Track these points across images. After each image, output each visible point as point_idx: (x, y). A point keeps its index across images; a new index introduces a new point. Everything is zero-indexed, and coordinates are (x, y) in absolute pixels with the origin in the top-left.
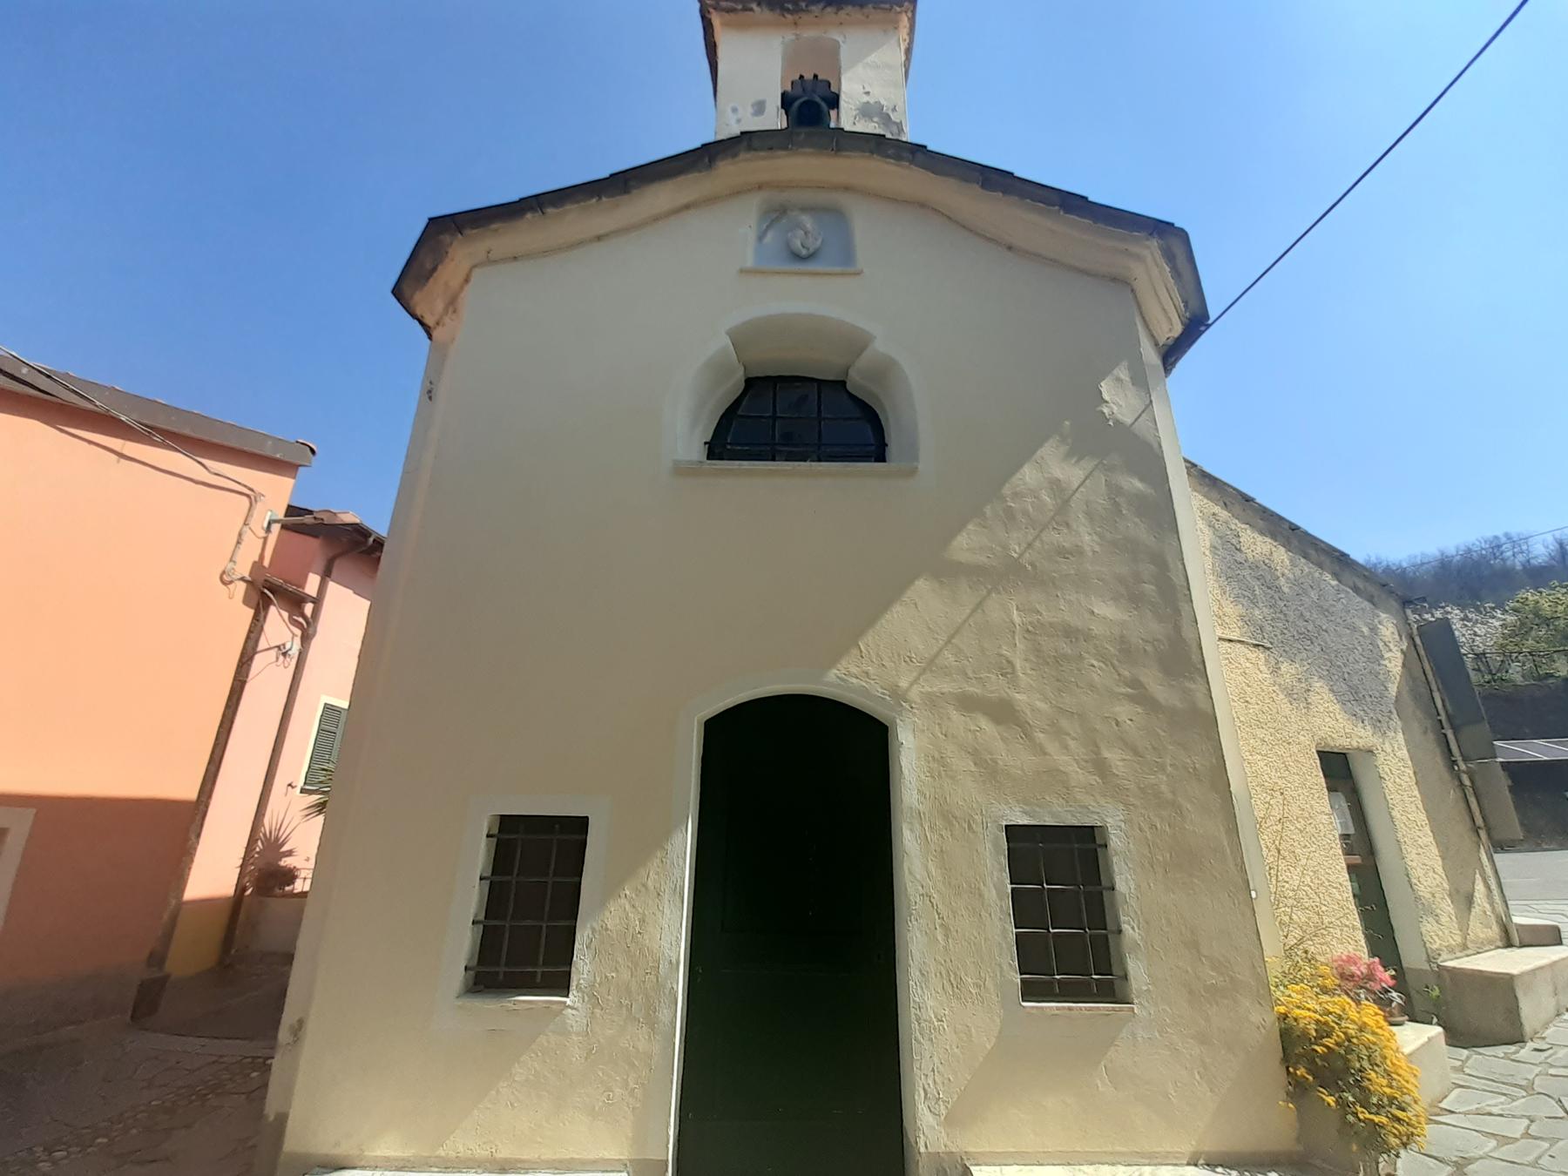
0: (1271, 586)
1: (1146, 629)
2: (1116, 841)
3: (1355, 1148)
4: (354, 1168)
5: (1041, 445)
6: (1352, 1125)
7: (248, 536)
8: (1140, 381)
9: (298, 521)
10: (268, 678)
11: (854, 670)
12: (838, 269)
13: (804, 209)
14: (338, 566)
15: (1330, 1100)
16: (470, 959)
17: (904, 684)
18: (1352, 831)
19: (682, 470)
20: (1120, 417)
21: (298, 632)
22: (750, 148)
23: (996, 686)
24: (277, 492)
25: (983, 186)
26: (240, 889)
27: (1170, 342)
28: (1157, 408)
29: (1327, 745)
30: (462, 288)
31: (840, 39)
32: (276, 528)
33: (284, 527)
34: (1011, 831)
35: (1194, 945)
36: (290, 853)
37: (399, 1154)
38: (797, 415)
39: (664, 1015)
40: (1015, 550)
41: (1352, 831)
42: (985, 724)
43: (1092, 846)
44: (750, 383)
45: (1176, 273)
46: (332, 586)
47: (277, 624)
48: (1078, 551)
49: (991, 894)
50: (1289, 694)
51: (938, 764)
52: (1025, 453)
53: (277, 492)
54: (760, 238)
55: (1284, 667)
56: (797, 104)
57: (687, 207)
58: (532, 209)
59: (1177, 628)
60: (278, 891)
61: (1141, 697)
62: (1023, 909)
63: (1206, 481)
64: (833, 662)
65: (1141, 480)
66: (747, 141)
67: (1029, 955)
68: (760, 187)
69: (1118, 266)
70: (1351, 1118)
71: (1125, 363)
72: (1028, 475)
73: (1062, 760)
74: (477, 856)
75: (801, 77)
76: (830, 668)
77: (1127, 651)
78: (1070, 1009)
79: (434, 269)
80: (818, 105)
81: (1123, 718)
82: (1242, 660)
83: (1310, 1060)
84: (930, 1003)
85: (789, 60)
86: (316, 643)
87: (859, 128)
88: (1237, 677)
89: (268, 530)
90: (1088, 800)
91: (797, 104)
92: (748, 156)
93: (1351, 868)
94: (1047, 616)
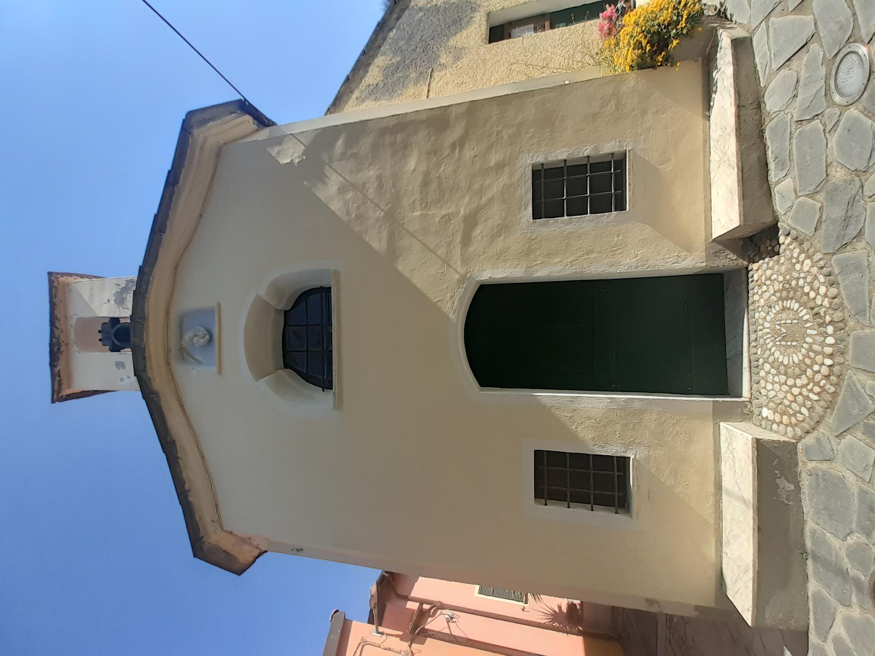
0: (397, 68)
1: (421, 140)
2: (540, 159)
3: (700, 29)
6: (689, 30)
7: (386, 645)
8: (279, 140)
9: (377, 618)
10: (466, 627)
11: (449, 305)
12: (216, 318)
13: (181, 337)
15: (675, 42)
17: (457, 276)
18: (532, 26)
19: (339, 404)
21: (439, 611)
22: (145, 370)
23: (457, 225)
24: (361, 630)
26: (579, 633)
27: (256, 122)
30: (236, 535)
31: (75, 318)
32: (381, 629)
33: (380, 624)
35: (595, 116)
36: (560, 607)
38: (303, 338)
39: (637, 405)
40: (379, 214)
41: (532, 26)
42: (477, 231)
44: (286, 366)
46: (414, 594)
48: (379, 178)
49: (570, 228)
50: (457, 58)
51: (500, 257)
52: (322, 207)
53: (360, 630)
54: (200, 363)
55: (442, 61)
57: (182, 406)
58: (186, 497)
61: (461, 143)
62: (576, 210)
65: (337, 140)
67: (601, 206)
68: (168, 363)
69: (212, 152)
70: (685, 31)
71: (269, 149)
72: (336, 206)
73: (495, 190)
74: (556, 511)
76: (448, 318)
77: (434, 152)
78: (630, 184)
79: (225, 551)
80: (117, 330)
81: (472, 154)
82: (439, 85)
83: (654, 54)
86: (445, 601)
89: (382, 633)
92: (149, 371)
94: (417, 196)
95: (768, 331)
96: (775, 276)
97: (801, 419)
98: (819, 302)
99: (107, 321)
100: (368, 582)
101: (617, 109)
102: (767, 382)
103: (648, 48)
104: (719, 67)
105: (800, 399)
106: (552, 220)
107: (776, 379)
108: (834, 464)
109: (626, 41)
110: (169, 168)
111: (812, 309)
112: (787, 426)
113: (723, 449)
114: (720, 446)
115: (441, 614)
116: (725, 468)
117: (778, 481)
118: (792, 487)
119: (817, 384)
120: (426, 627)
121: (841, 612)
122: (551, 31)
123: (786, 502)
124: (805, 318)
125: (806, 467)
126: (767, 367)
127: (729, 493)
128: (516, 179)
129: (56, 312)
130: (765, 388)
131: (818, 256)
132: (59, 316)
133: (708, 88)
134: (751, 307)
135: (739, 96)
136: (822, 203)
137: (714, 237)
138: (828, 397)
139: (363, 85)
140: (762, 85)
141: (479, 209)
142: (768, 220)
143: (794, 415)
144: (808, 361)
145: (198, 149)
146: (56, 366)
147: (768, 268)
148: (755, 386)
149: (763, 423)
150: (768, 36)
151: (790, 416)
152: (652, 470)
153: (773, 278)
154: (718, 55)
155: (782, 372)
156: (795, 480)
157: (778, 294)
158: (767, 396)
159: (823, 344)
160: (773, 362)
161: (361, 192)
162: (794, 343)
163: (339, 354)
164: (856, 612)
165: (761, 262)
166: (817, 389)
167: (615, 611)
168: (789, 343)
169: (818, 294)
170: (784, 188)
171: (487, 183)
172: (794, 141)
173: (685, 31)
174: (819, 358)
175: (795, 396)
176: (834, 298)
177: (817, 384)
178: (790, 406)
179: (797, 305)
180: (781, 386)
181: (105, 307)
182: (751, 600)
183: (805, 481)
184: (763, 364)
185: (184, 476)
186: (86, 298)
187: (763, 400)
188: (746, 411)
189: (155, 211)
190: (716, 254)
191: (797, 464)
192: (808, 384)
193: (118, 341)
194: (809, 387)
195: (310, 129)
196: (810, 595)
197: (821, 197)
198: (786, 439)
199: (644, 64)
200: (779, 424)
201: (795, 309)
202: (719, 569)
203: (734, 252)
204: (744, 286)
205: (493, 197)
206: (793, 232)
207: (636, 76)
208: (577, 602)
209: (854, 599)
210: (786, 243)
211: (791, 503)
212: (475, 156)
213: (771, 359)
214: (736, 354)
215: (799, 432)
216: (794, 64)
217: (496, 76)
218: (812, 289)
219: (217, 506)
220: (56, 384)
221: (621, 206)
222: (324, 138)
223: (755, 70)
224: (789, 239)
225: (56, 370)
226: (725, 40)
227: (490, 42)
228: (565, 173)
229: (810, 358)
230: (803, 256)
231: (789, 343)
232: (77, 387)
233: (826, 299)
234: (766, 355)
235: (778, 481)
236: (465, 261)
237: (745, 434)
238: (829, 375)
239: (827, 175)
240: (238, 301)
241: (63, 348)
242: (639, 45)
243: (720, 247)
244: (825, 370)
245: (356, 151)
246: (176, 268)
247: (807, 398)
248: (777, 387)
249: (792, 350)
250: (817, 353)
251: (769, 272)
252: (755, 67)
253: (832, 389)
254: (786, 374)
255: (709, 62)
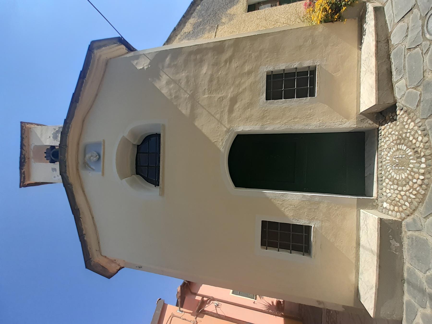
0: (200, 24)
1: (210, 57)
2: (271, 69)
3: (357, 2)
4: (358, 286)
5: (156, 87)
6: (351, 3)
7: (183, 317)
8: (137, 57)
9: (181, 303)
10: (225, 310)
11: (221, 143)
12: (102, 147)
13: (85, 156)
14: (193, 291)
15: (344, 8)
16: (301, 254)
17: (225, 129)
18: (270, 5)
19: (162, 193)
20: (148, 63)
21: (212, 301)
22: (65, 172)
23: (226, 102)
24: (172, 309)
25: (78, 103)
26: (282, 316)
27: (127, 49)
28: (146, 52)
29: (246, 10)
30: (108, 258)
31: (33, 145)
32: (181, 309)
33: (182, 307)
34: (267, 99)
35: (300, 47)
36: (273, 302)
37: (354, 274)
38: (146, 159)
39: (317, 199)
40: (187, 96)
41: (270, 5)
42: (237, 106)
43: (272, 76)
44: (137, 173)
45: (105, 46)
46: (199, 292)
47: (210, 308)
48: (187, 77)
49: (285, 105)
50: (230, 20)
51: (248, 119)
52: (159, 92)
53: (172, 309)
54: (94, 170)
55: (223, 21)
56: (53, 158)
57: (84, 191)
58: (84, 238)
59: (210, 49)
60: (283, 305)
61: (230, 60)
62: (289, 95)
63: (169, 41)
64: (219, 150)
65: (166, 57)
66: (63, 173)
67: (302, 94)
68: (77, 170)
69: (104, 62)
70: (349, 3)
71: (132, 62)
72: (165, 91)
73: (247, 84)
74: (272, 253)
75: (45, 157)
76: (220, 150)
77: (216, 64)
78: (317, 83)
79: (103, 267)
80: (53, 152)
81: (236, 65)
82: (221, 33)
83: (333, 14)
84: (315, 123)
85: (41, 161)
86: (215, 297)
87: (59, 139)
88: (225, 33)
89: (182, 311)
90: (259, 76)
91: (53, 158)
92: (68, 172)
93: (280, 4)
94: (206, 87)
95: (389, 161)
96: (393, 132)
97: (405, 208)
98: (417, 145)
99: (49, 147)
100: (176, 285)
101: (312, 43)
102: (386, 188)
103: (330, 11)
104: (367, 22)
105: (405, 198)
106: (276, 101)
107: (392, 187)
108: (422, 233)
109: (318, 8)
110: (81, 70)
111: (414, 149)
112: (397, 212)
113: (362, 222)
114: (360, 222)
115: (213, 303)
116: (362, 234)
117: (391, 241)
118: (398, 245)
119: (415, 189)
120: (205, 309)
121: (421, 311)
122: (279, 6)
123: (395, 252)
124: (409, 154)
125: (407, 234)
126: (387, 181)
127: (364, 247)
128: (258, 79)
129: (23, 142)
130: (385, 192)
131: (418, 120)
132: (25, 144)
133: (361, 33)
134: (379, 149)
135: (377, 34)
136: (421, 92)
137: (361, 112)
138: (421, 197)
139: (182, 33)
140: (390, 31)
141: (238, 94)
142: (391, 101)
143: (401, 206)
144: (410, 177)
145: (96, 61)
146: (22, 169)
147: (390, 128)
148: (380, 191)
149: (384, 210)
150: (392, 6)
151: (399, 207)
152: (323, 233)
153: (392, 133)
154: (367, 16)
155: (396, 183)
156: (400, 241)
157: (395, 142)
158: (386, 196)
159: (419, 168)
160: (391, 178)
161: (178, 84)
162: (403, 168)
163: (163, 167)
164: (428, 311)
165: (386, 125)
166: (415, 192)
167: (301, 306)
168: (400, 168)
169: (417, 141)
170: (401, 85)
171: (243, 81)
172: (406, 59)
173: (349, 3)
174: (416, 176)
175: (402, 196)
176: (426, 143)
177: (415, 189)
178: (399, 201)
179: (405, 147)
180: (394, 190)
181: (48, 140)
182: (373, 304)
183: (406, 242)
184: (385, 179)
185: (83, 227)
186: (39, 135)
187: (384, 198)
188: (374, 204)
189: (73, 91)
190: (362, 121)
191: (401, 233)
192: (410, 190)
193: (54, 157)
194: (410, 191)
195: (153, 51)
196: (404, 302)
197: (420, 88)
198: (396, 219)
199: (328, 19)
200: (392, 211)
201: (404, 149)
202: (357, 285)
203: (371, 120)
204: (376, 138)
205: (246, 88)
206: (405, 108)
207: (323, 26)
208: (281, 300)
209: (428, 304)
210: (400, 114)
211: (397, 253)
212: (237, 67)
213: (390, 176)
214: (370, 174)
215: (403, 215)
216: (406, 19)
217: (250, 28)
218: (414, 138)
219: (99, 243)
220: (22, 178)
221: (312, 94)
222: (160, 56)
223: (386, 23)
224: (402, 112)
225: (23, 171)
226: (370, 8)
227: (248, 12)
228: (284, 77)
229: (411, 175)
230: (410, 120)
231: (400, 168)
232: (32, 181)
233: (422, 144)
234: (387, 175)
235: (391, 241)
236: (230, 121)
237: (374, 216)
238: (422, 185)
239: (424, 77)
240: (113, 139)
241: (26, 161)
242: (325, 10)
243: (364, 117)
244: (419, 182)
245: (176, 63)
246: (83, 121)
247: (409, 197)
248: (392, 191)
249: (402, 171)
250: (415, 173)
251: (390, 130)
252: (386, 21)
253: (423, 192)
254: (397, 184)
255: (361, 19)
